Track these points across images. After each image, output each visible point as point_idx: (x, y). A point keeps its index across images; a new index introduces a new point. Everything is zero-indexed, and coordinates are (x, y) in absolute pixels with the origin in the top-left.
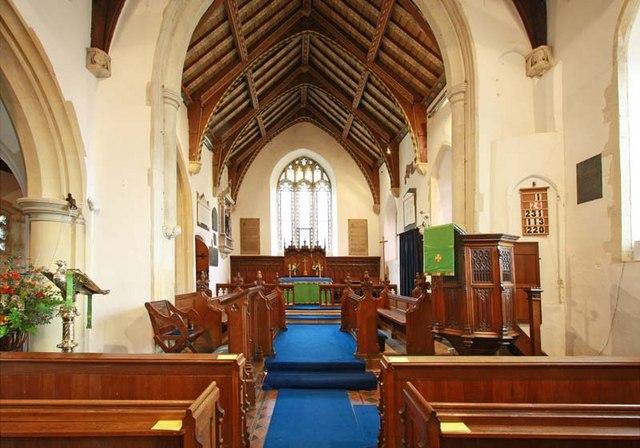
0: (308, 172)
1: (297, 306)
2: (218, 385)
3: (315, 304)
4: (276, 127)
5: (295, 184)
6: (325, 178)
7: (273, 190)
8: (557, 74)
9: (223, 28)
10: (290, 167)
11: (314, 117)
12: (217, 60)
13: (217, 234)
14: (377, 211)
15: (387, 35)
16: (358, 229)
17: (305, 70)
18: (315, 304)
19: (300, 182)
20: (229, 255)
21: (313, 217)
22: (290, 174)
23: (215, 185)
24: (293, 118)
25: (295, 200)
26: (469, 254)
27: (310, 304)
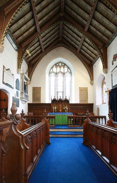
0: (62, 68)
1: (56, 126)
3: (65, 125)
6: (69, 71)
7: (47, 75)
9: (38, 44)
10: (55, 66)
11: (65, 44)
12: (36, 52)
13: (19, 92)
14: (92, 84)
15: (91, 24)
16: (83, 92)
18: (65, 125)
19: (59, 73)
20: (27, 103)
21: (64, 87)
22: (54, 69)
23: (18, 68)
24: (56, 45)
25: (56, 80)
27: (62, 125)
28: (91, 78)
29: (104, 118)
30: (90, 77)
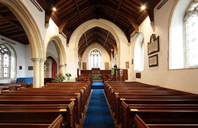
0: (96, 52)
2: (62, 116)
4: (89, 44)
5: (94, 55)
7: (89, 56)
8: (131, 47)
9: (73, 4)
14: (111, 61)
16: (107, 64)
17: (96, 35)
22: (93, 53)
25: (94, 59)
26: (116, 71)
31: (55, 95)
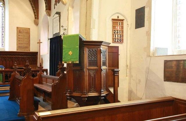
14: (37, 24)
26: (86, 51)
28: (35, 15)
29: (45, 72)
30: (34, 13)
31: (55, 62)
